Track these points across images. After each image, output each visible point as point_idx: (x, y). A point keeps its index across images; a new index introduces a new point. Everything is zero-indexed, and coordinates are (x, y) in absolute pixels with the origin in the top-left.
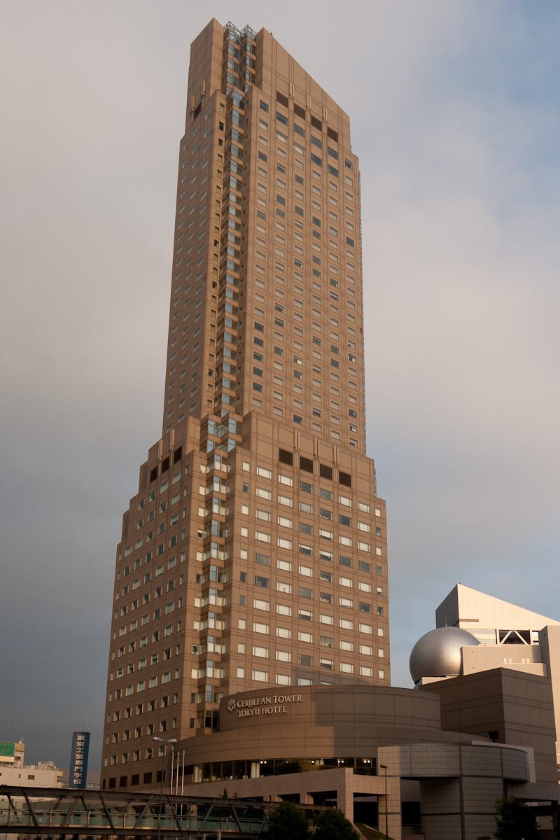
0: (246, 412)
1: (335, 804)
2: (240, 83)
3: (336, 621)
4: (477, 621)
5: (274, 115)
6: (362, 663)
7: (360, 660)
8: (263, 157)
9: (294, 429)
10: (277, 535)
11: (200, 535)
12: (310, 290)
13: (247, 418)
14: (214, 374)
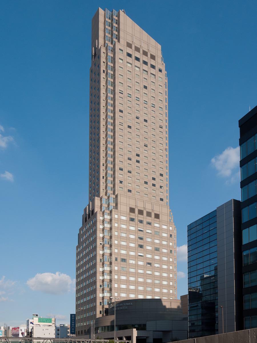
5: (126, 54)
6: (163, 288)
11: (101, 244)
13: (117, 196)
14: (105, 178)
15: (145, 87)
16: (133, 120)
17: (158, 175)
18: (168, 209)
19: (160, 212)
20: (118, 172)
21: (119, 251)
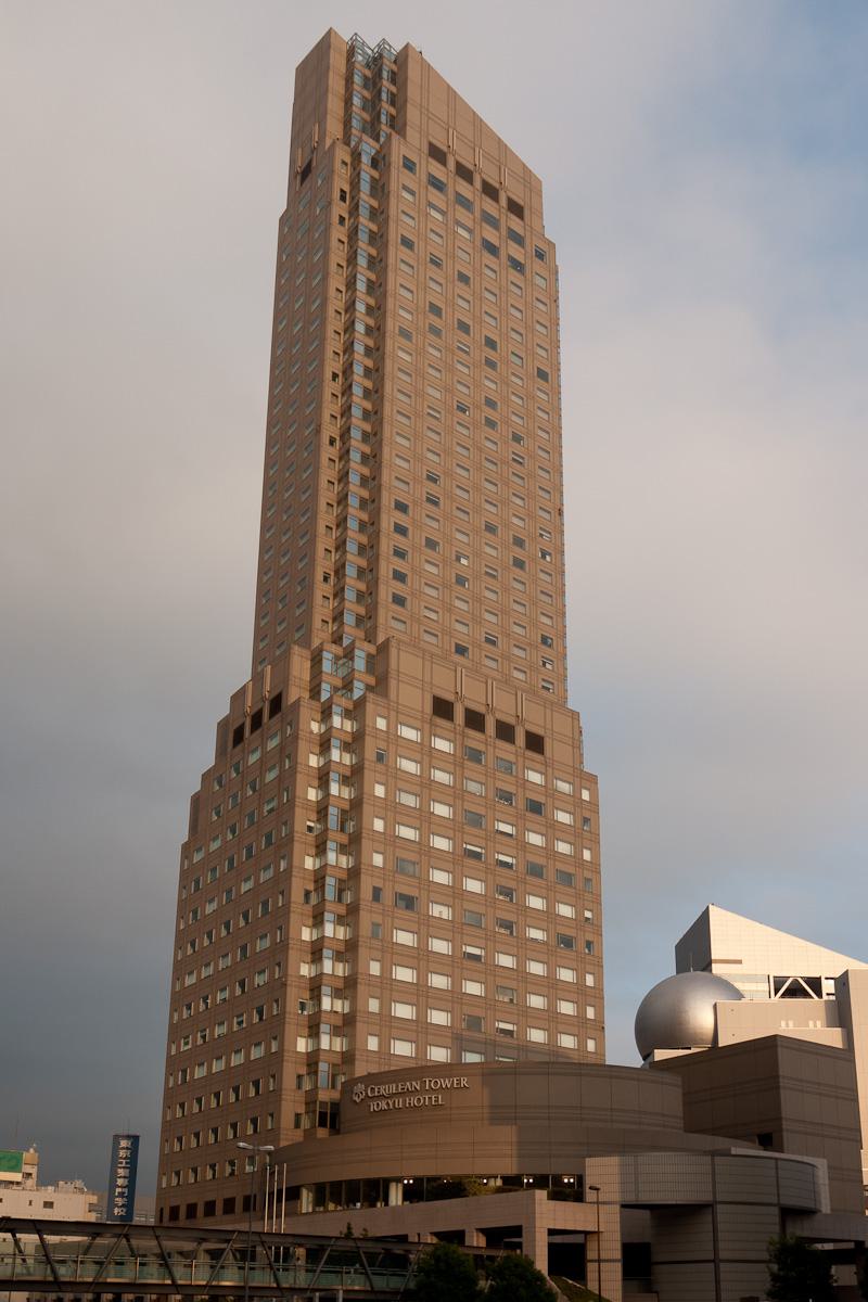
0: (381, 639)
1: (519, 1246)
2: (372, 129)
3: (521, 963)
4: (740, 962)
5: (424, 178)
6: (561, 1028)
7: (557, 1023)
8: (407, 243)
9: (456, 664)
10: (429, 829)
11: (310, 829)
12: (480, 450)
13: (384, 649)
14: (332, 580)
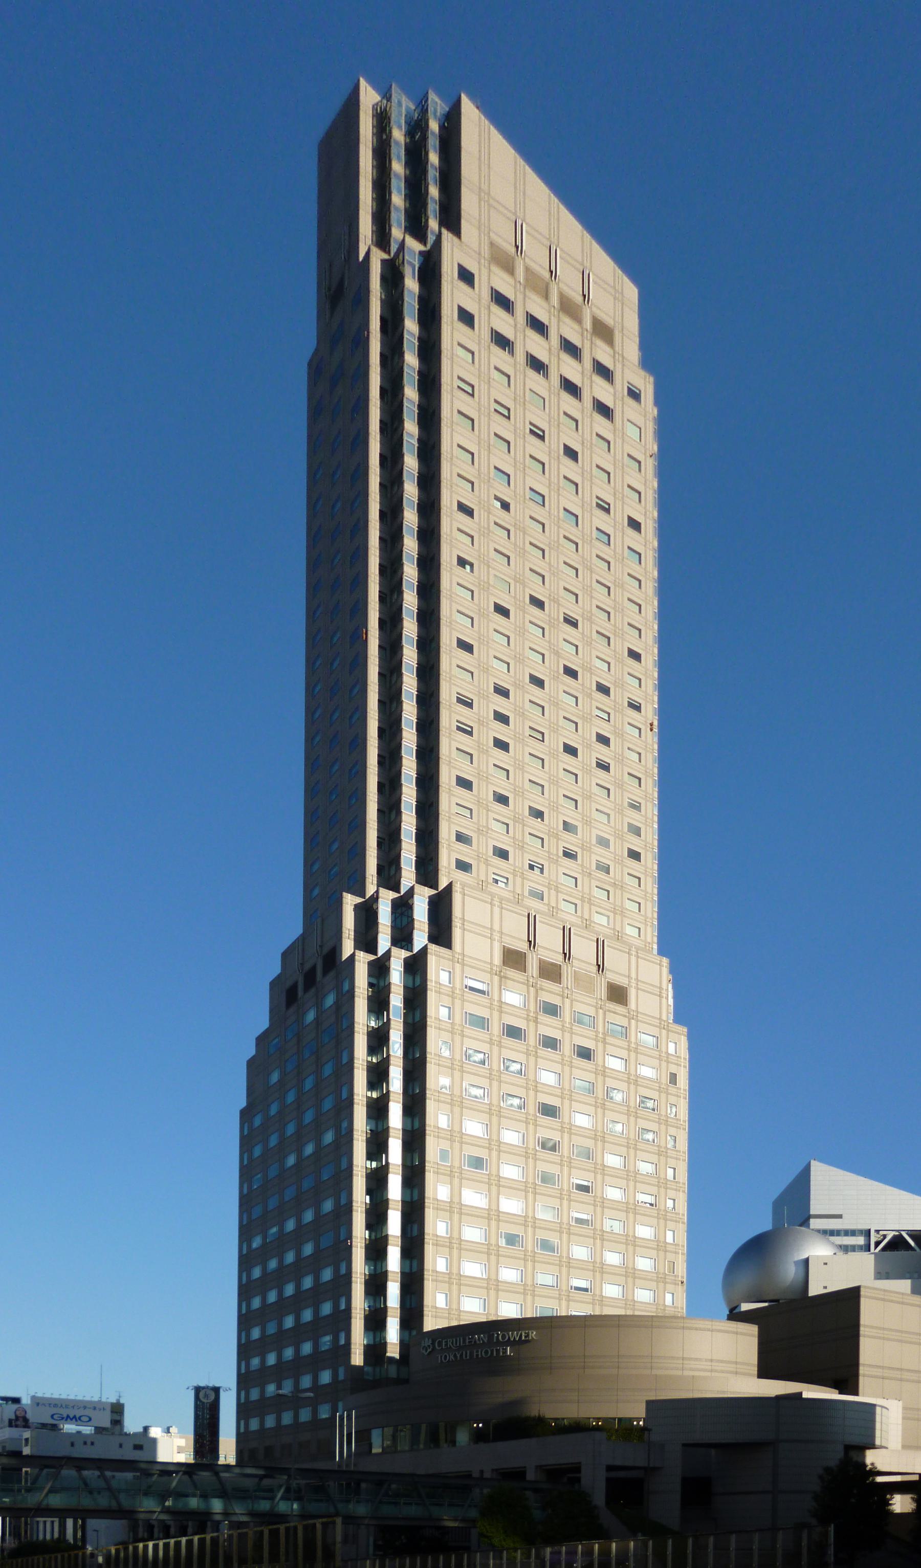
0: (443, 884)
1: (578, 1480)
2: (417, 228)
3: (494, 1201)
4: (840, 1216)
9: (492, 895)
12: (557, 654)
15: (571, 454)
16: (516, 581)
17: (619, 852)
18: (665, 970)
19: (629, 977)
20: (450, 793)
21: (456, 1194)
